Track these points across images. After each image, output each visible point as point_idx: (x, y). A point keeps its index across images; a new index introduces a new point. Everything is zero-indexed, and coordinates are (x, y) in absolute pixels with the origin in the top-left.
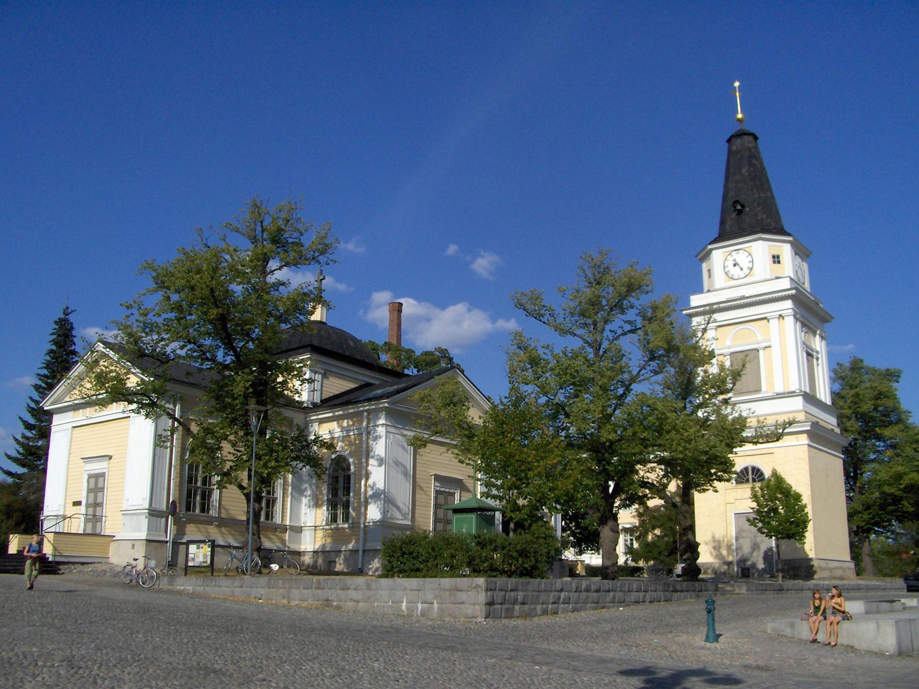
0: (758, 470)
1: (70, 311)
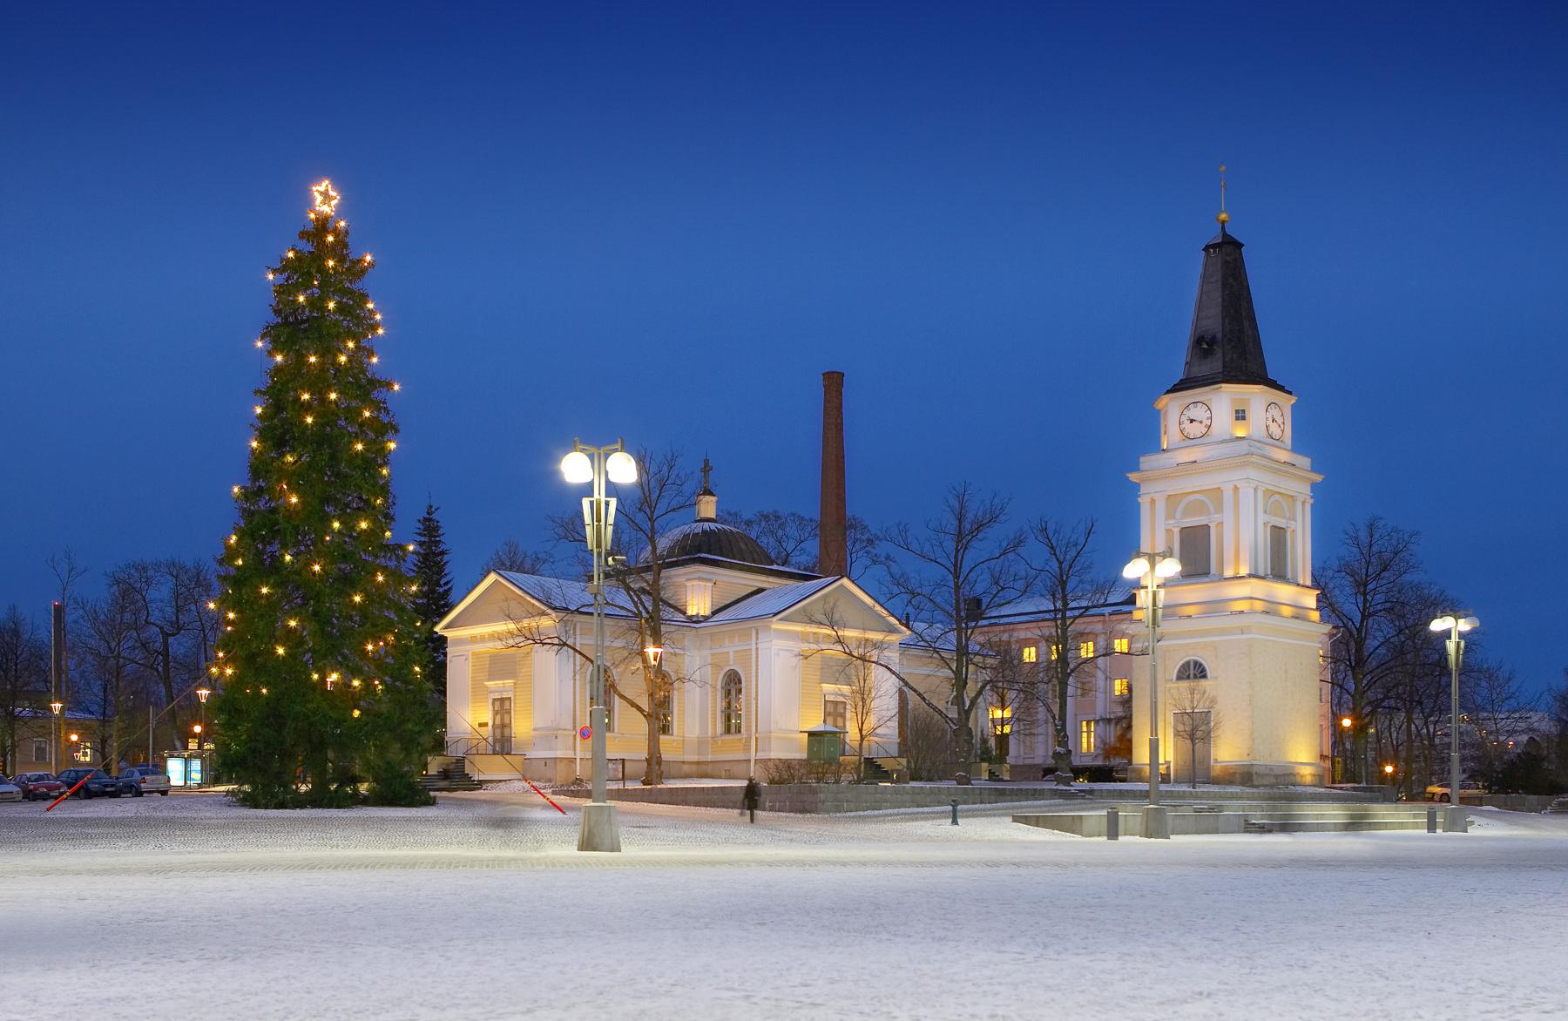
0: (1201, 665)
1: (433, 509)
